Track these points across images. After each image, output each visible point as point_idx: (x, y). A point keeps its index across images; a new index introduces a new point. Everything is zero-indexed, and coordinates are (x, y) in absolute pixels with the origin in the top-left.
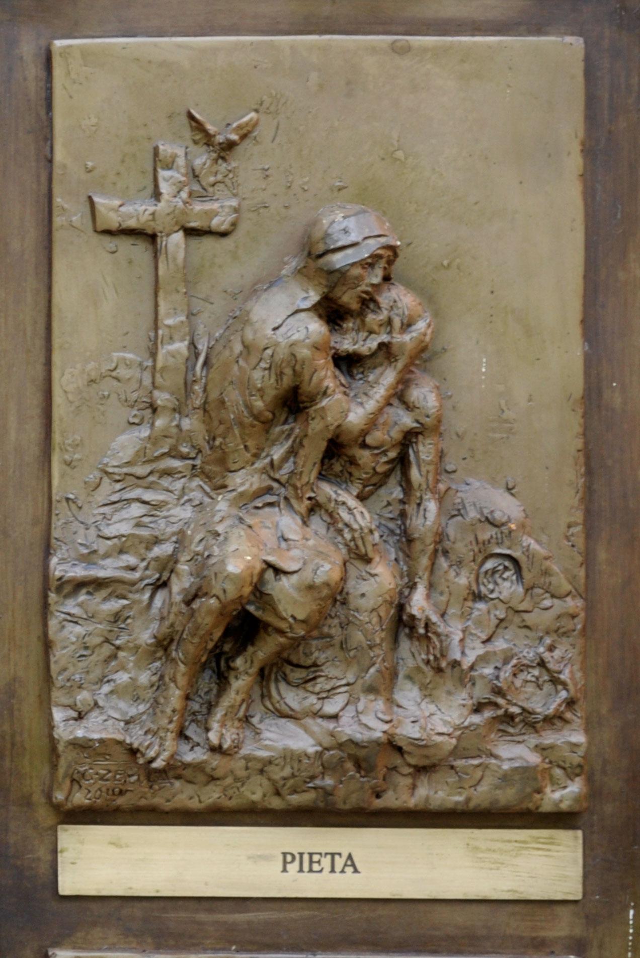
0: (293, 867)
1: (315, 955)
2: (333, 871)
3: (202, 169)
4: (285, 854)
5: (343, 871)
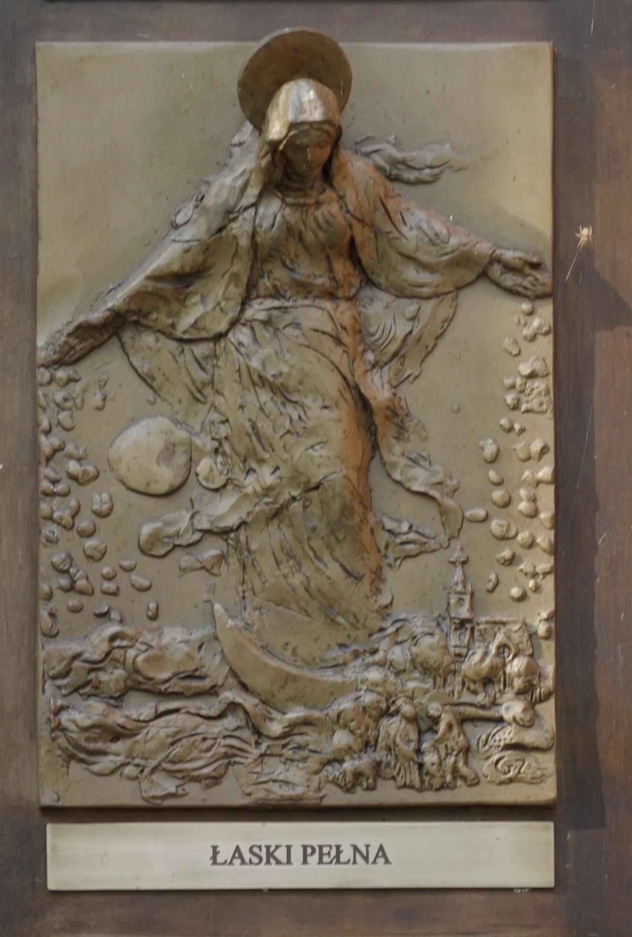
0: (313, 859)
1: (475, 726)
2: (289, 848)
3: (355, 211)
4: (305, 848)
5: (374, 862)
